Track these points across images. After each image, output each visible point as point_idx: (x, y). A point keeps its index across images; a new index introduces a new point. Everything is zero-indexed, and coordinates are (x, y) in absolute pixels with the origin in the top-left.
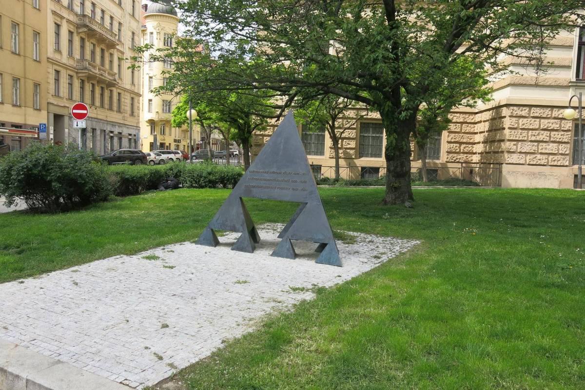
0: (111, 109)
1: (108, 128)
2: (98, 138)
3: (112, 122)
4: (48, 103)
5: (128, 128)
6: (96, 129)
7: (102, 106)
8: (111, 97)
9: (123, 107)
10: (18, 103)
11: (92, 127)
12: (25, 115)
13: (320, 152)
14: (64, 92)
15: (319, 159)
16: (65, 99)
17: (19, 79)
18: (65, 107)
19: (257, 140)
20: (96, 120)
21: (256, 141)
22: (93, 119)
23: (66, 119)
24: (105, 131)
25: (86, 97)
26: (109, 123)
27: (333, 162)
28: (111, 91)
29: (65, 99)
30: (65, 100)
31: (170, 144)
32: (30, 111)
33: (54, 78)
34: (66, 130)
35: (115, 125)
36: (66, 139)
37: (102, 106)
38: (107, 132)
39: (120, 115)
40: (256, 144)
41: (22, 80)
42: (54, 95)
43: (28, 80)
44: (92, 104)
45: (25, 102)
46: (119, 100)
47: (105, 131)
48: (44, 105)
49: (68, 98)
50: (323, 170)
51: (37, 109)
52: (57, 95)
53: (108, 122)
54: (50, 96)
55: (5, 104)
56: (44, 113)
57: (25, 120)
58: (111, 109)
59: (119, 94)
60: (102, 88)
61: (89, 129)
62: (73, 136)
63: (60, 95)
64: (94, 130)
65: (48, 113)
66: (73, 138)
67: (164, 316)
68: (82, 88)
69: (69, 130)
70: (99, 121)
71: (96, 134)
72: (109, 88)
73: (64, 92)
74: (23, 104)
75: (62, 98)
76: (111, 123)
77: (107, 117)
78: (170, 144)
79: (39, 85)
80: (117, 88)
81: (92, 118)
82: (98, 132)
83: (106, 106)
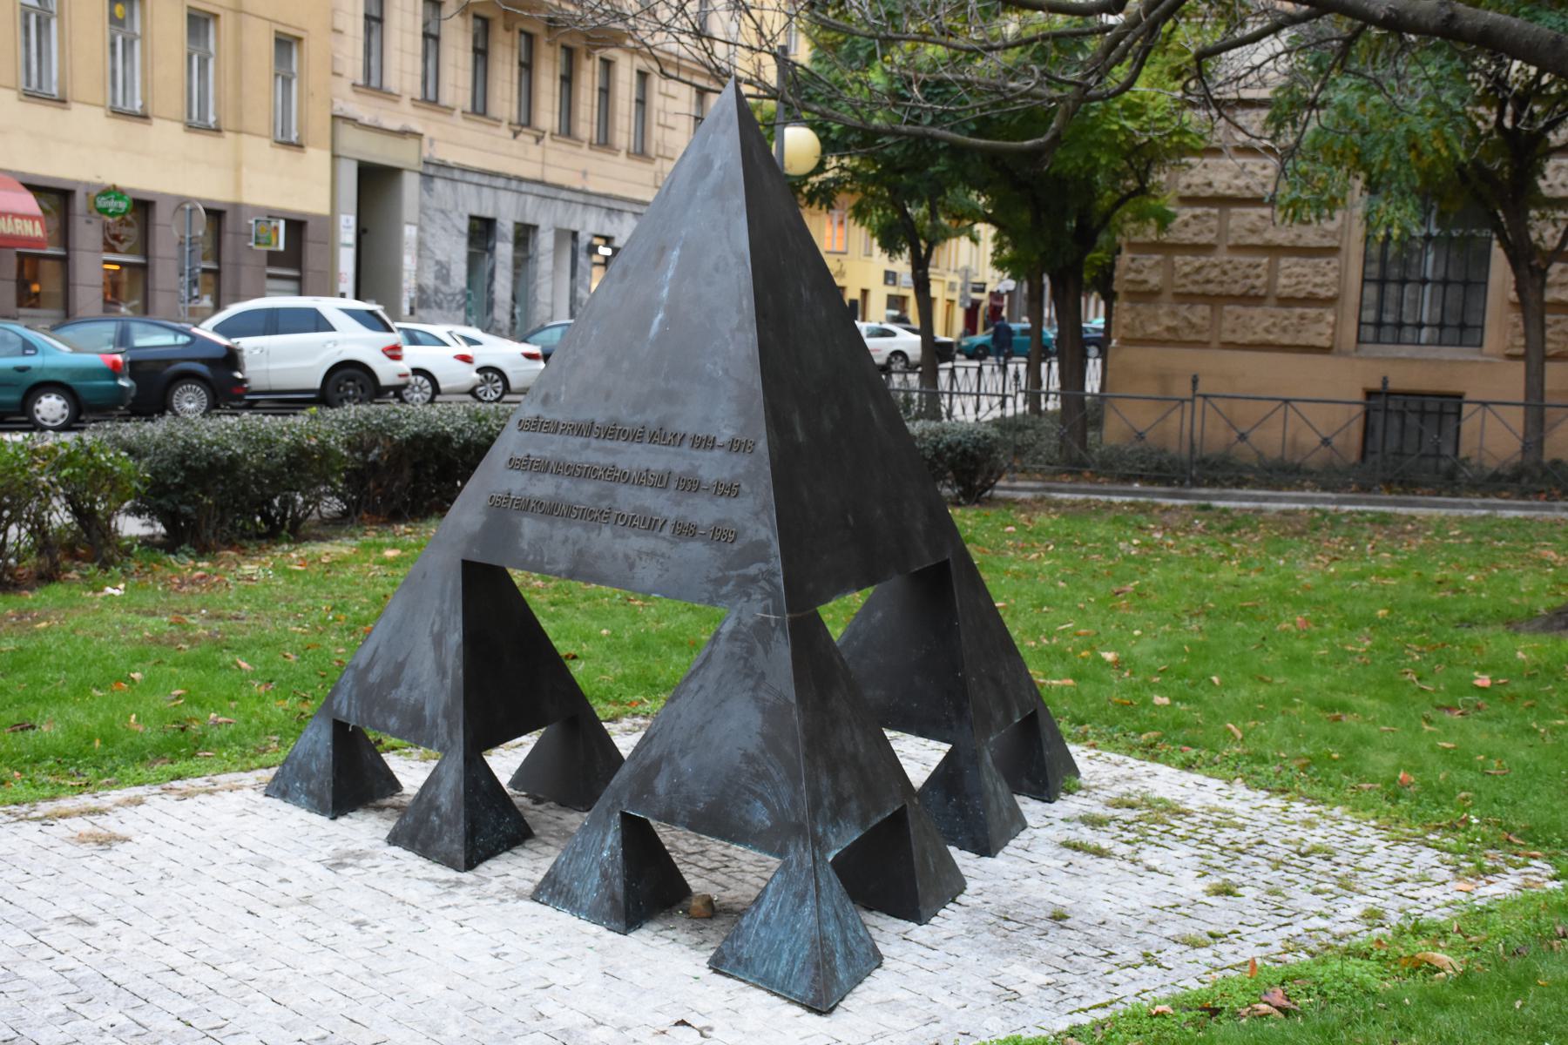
0: (604, 142)
1: (589, 224)
2: (545, 263)
3: (607, 197)
4: (334, 117)
5: (610, 210)
6: (535, 228)
7: (567, 130)
8: (606, 92)
9: (656, 133)
10: (212, 119)
11: (518, 220)
12: (238, 167)
13: (1463, 326)
14: (402, 71)
15: (1452, 362)
16: (458, 112)
17: (216, 16)
18: (404, 133)
19: (1139, 271)
20: (537, 189)
21: (1131, 276)
22: (524, 187)
23: (411, 185)
24: (575, 235)
25: (498, 93)
26: (594, 200)
27: (1512, 380)
28: (608, 64)
29: (458, 112)
30: (406, 104)
31: (865, 292)
32: (259, 150)
33: (361, 12)
34: (410, 232)
35: (621, 211)
36: (409, 261)
37: (567, 130)
38: (584, 239)
39: (646, 166)
40: (1131, 288)
41: (227, 21)
42: (418, 97)
43: (252, 20)
44: (524, 120)
45: (239, 117)
46: (642, 102)
47: (575, 235)
48: (319, 124)
49: (418, 95)
50: (1471, 421)
51: (288, 144)
52: (372, 83)
53: (589, 199)
54: (344, 87)
55: (228, 135)
56: (317, 158)
57: (238, 185)
58: (604, 142)
59: (643, 76)
60: (570, 53)
61: (506, 227)
62: (440, 256)
63: (386, 84)
64: (525, 234)
65: (335, 157)
66: (438, 263)
67: (279, 965)
68: (481, 54)
69: (421, 229)
70: (552, 192)
71: (536, 248)
72: (598, 54)
73: (402, 71)
74: (228, 122)
75: (449, 110)
76: (604, 203)
77: (585, 174)
78: (865, 292)
79: (299, 40)
80: (635, 51)
81: (521, 180)
82: (545, 240)
83: (586, 125)
